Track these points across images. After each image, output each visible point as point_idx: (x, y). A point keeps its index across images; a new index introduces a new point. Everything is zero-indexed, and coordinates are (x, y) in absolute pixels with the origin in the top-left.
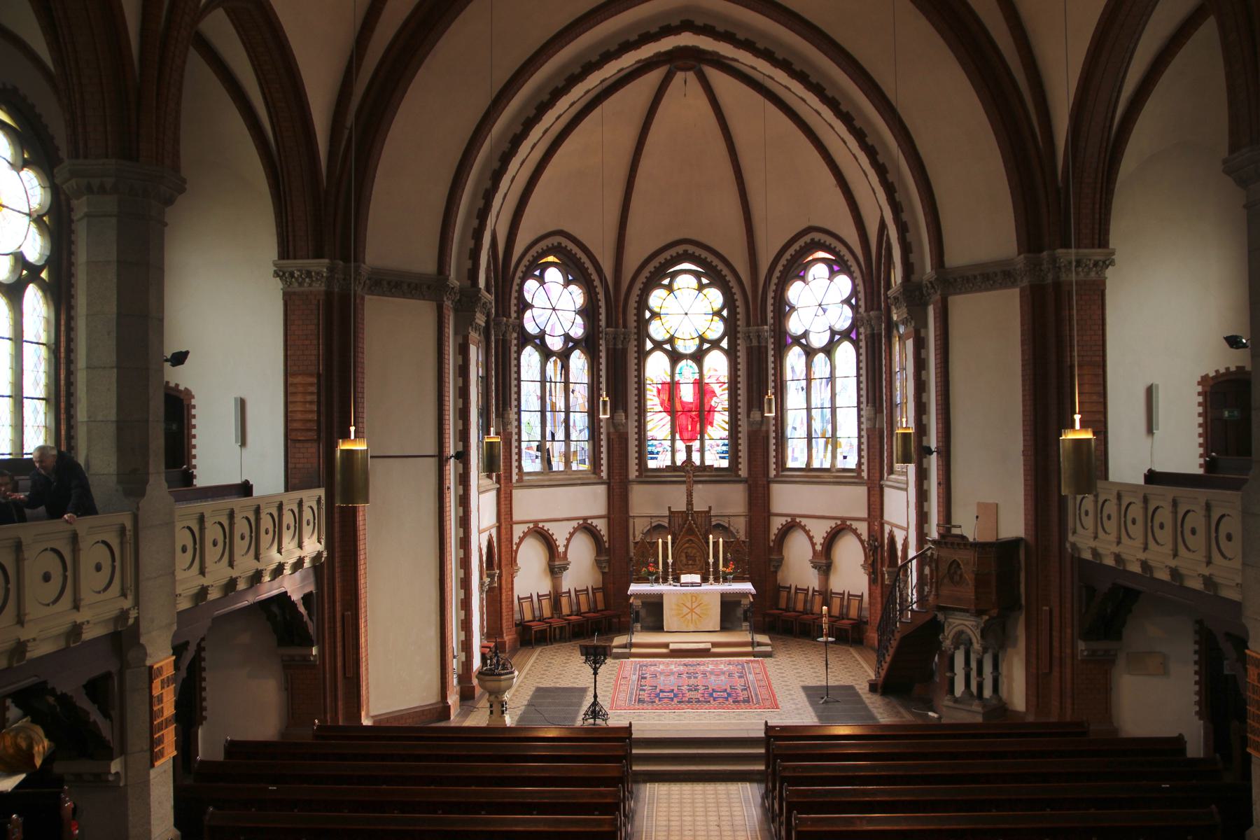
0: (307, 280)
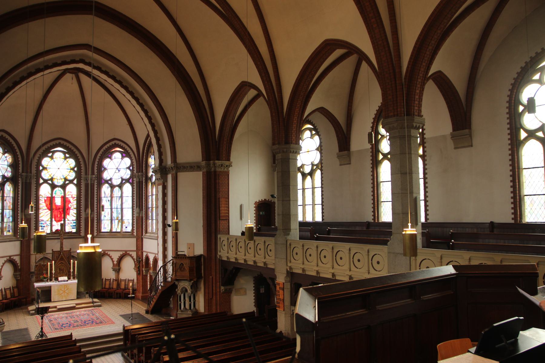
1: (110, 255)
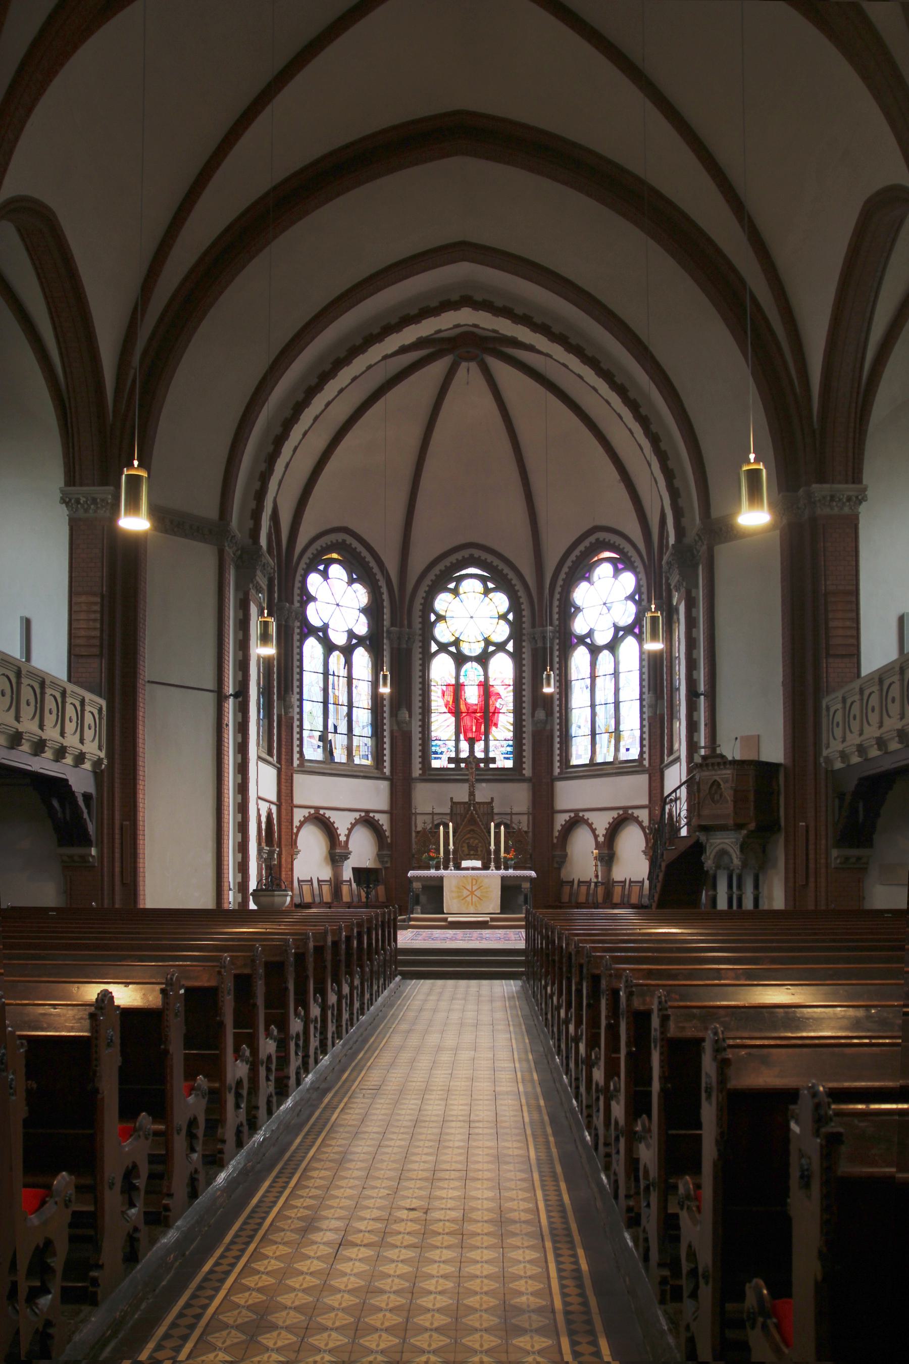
0: (92, 506)
1: (590, 821)
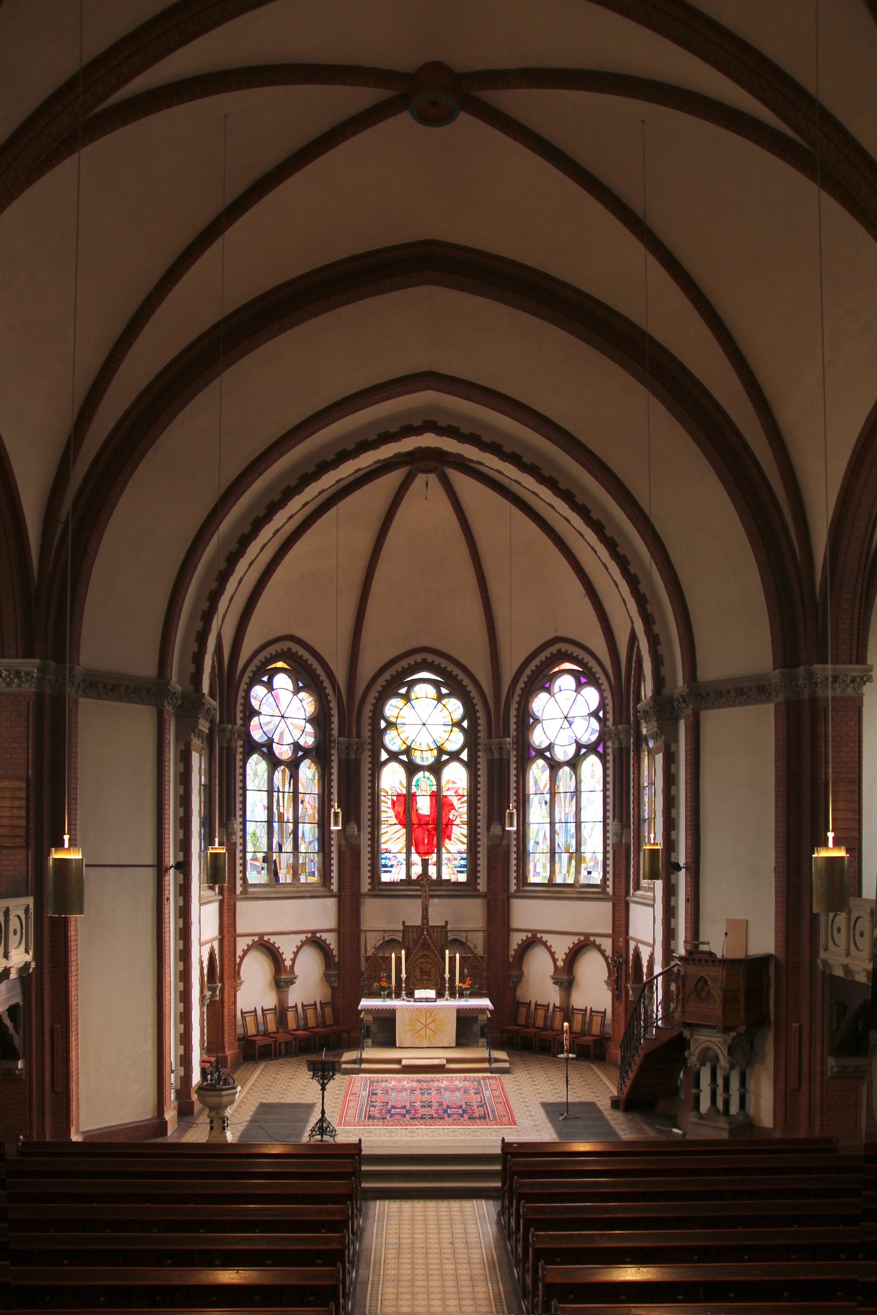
0: (16, 680)
1: (548, 944)
